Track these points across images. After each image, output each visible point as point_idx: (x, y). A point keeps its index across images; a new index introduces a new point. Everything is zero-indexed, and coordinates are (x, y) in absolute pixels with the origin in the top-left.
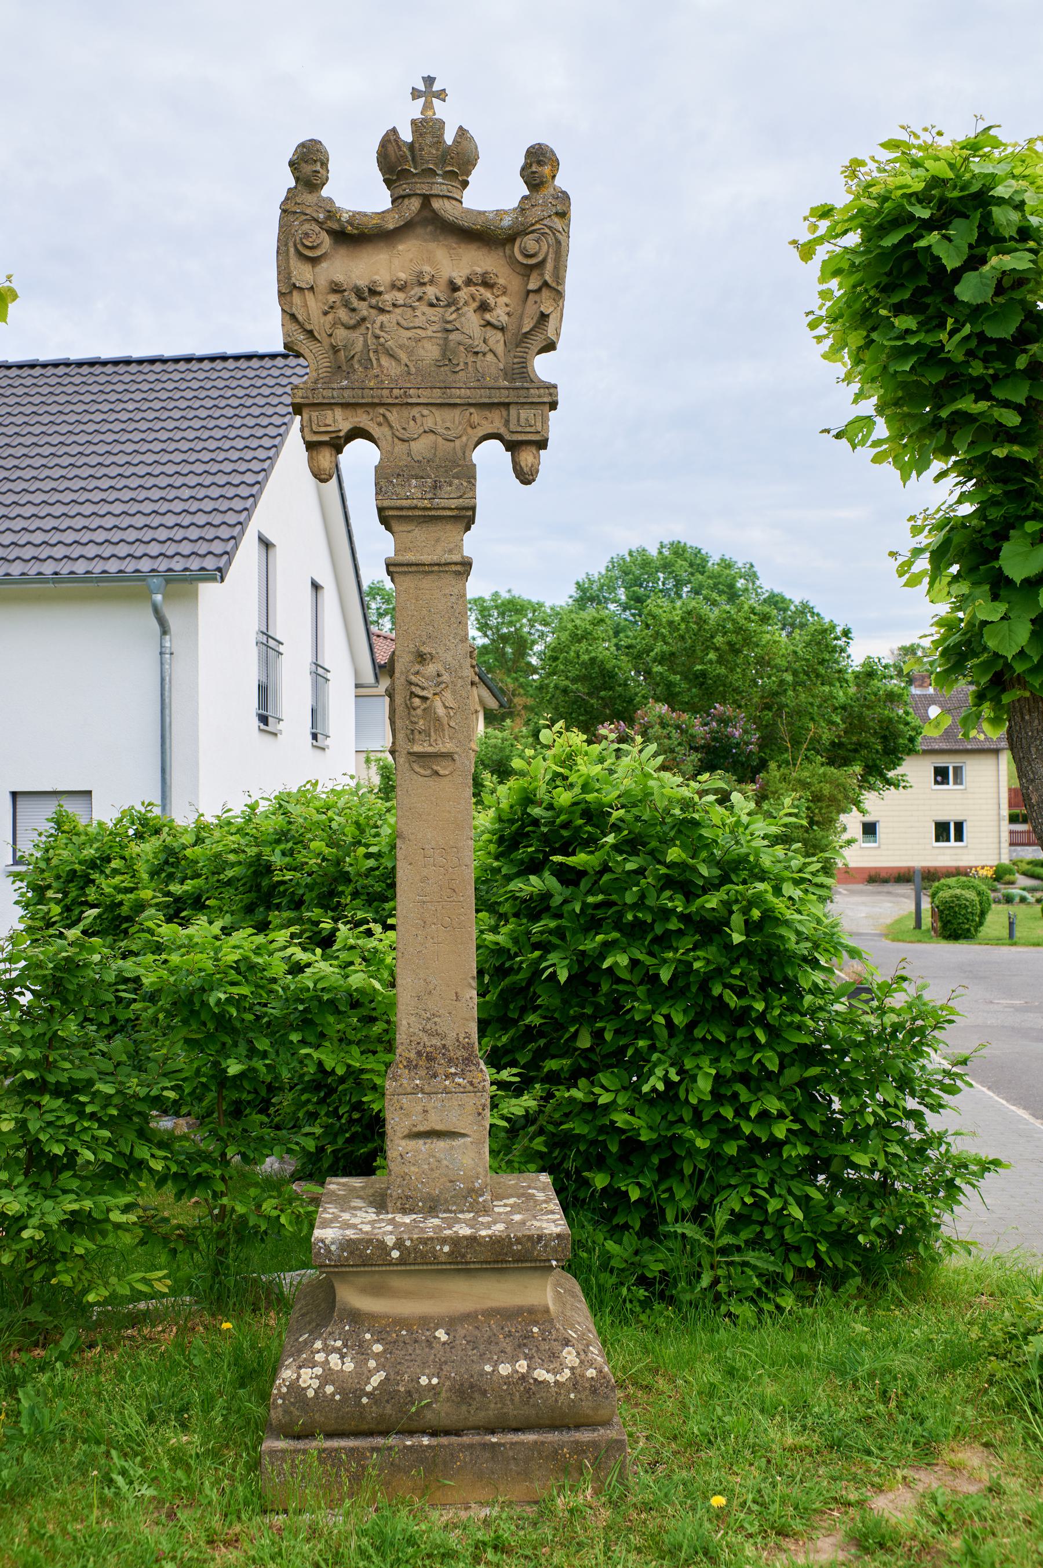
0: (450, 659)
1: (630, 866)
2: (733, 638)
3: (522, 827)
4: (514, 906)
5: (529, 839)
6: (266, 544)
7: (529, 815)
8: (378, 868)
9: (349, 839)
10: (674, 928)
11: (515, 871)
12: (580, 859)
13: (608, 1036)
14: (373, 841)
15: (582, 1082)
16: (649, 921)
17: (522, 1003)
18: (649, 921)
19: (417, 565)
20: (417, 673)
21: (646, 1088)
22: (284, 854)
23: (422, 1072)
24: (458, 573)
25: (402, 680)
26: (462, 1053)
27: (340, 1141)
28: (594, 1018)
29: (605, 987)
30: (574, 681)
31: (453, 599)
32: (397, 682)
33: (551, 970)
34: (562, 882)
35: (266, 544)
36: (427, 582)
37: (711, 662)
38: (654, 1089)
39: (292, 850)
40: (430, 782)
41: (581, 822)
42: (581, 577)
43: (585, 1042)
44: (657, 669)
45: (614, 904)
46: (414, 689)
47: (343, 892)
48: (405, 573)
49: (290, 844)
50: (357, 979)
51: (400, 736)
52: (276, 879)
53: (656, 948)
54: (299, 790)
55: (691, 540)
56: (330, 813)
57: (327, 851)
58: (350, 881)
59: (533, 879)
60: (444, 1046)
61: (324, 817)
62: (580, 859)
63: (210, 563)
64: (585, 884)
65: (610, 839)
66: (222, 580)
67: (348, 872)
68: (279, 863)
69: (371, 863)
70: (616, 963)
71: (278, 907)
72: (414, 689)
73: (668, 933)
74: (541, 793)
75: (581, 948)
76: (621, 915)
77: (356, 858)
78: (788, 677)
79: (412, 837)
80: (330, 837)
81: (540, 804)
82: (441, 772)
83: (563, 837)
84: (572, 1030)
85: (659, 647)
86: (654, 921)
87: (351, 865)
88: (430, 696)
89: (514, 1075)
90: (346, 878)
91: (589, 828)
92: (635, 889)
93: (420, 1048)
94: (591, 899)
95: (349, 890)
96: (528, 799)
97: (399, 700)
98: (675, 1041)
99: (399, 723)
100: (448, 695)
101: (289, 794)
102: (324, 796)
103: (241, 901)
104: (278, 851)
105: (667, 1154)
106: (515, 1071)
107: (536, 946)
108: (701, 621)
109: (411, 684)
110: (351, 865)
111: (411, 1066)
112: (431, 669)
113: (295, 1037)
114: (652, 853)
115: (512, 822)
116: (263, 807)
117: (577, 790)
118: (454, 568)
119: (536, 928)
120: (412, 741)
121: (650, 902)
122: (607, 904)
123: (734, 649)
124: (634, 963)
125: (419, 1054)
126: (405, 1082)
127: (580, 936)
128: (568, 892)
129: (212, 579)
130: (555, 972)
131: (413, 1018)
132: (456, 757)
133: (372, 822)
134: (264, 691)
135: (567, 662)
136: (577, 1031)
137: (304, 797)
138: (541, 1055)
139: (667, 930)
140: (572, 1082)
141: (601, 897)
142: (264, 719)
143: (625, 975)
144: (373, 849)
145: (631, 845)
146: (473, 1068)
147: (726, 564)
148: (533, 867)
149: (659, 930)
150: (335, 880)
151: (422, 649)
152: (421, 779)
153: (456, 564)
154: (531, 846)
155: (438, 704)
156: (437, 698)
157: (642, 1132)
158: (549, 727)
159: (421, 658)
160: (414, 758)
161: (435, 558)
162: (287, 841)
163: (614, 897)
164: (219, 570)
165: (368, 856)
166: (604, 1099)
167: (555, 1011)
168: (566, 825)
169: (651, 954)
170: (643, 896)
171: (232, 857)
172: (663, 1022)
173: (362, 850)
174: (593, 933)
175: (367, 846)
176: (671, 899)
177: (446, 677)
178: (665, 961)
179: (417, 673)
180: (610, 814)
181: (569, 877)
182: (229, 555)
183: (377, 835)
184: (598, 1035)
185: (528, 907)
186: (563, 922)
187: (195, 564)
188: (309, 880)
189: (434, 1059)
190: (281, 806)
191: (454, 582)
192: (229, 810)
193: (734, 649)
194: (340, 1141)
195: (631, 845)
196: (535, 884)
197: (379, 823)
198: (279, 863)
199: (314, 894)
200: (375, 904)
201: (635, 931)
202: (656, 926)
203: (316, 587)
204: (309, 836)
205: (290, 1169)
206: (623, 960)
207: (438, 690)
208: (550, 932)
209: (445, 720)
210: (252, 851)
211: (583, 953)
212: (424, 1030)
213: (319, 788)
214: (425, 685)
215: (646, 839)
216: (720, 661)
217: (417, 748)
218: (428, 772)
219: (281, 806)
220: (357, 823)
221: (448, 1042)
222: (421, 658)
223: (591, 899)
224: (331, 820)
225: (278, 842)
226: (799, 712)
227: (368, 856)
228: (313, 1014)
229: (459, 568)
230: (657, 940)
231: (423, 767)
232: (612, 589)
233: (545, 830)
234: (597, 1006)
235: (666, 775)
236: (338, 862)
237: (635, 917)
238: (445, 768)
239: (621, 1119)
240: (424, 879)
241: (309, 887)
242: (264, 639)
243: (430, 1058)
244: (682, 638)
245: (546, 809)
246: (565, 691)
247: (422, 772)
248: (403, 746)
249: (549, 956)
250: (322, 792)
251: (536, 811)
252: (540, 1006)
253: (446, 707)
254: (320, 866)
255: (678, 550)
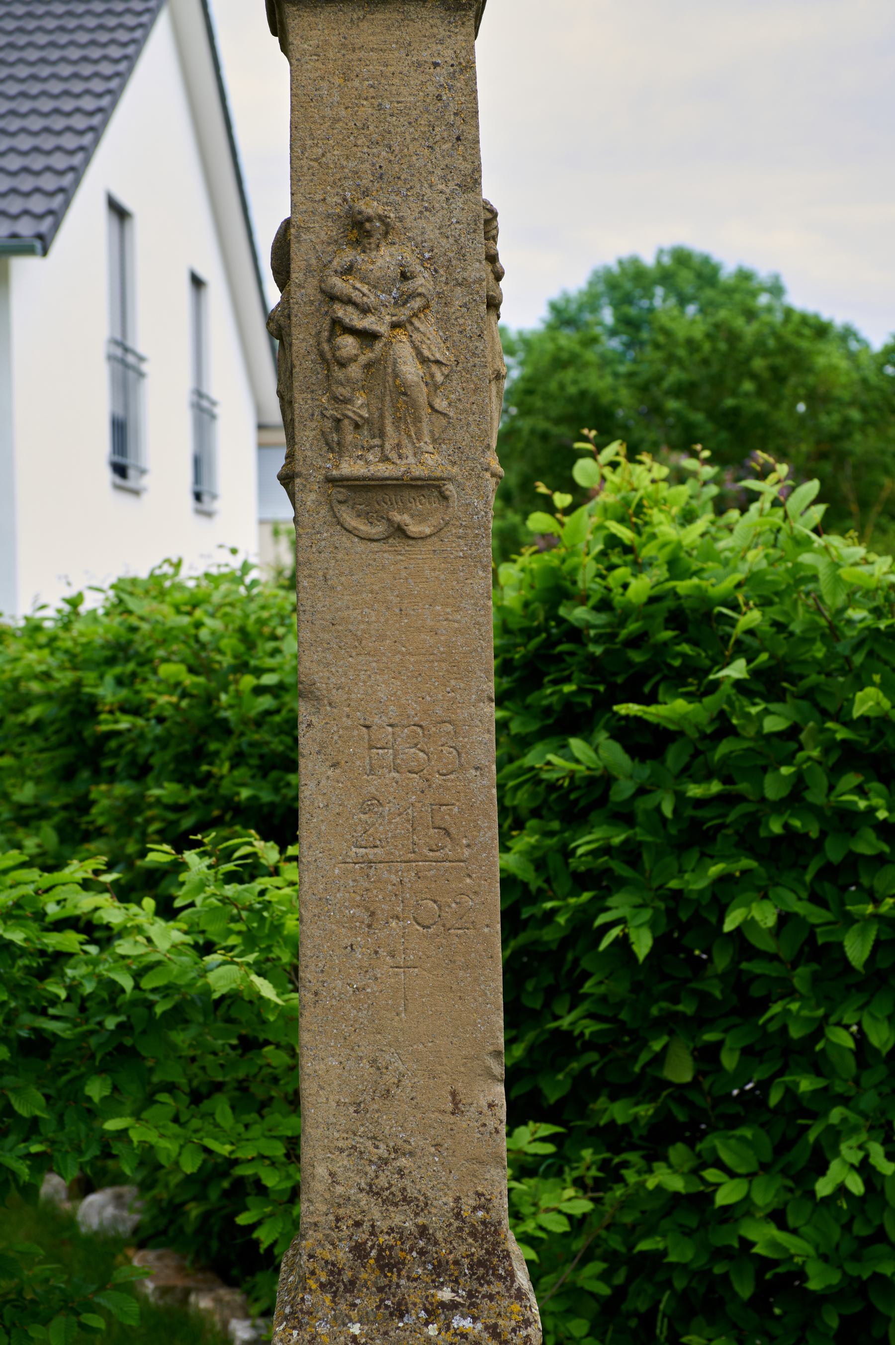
0: (432, 234)
1: (773, 724)
2: (779, 361)
3: (550, 643)
4: (533, 795)
5: (563, 667)
6: (119, 212)
7: (561, 621)
8: (278, 711)
9: (227, 661)
10: (868, 851)
11: (534, 727)
12: (672, 709)
13: (729, 1061)
14: (270, 662)
15: (678, 1152)
16: (814, 834)
17: (549, 980)
18: (814, 834)
20: (348, 270)
21: (824, 1187)
22: (120, 682)
23: (368, 1302)
26: (468, 1248)
27: (214, 1194)
28: (701, 1022)
29: (721, 962)
30: (558, 421)
31: (441, 75)
32: (297, 294)
33: (615, 932)
34: (632, 750)
35: (119, 212)
37: (747, 395)
38: (842, 1190)
39: (134, 675)
41: (668, 634)
42: (554, 294)
43: (681, 1070)
44: (672, 404)
45: (740, 798)
47: (217, 753)
49: (131, 666)
50: (223, 976)
51: (307, 435)
52: (104, 728)
53: (828, 890)
54: (152, 575)
55: (699, 243)
56: (198, 613)
57: (189, 680)
58: (229, 732)
59: (576, 744)
60: (423, 1230)
61: (186, 620)
62: (672, 709)
63: (26, 228)
64: (674, 757)
65: (737, 670)
66: (45, 252)
67: (225, 720)
68: (109, 699)
69: (266, 702)
70: (750, 923)
71: (112, 776)
73: (853, 861)
75: (673, 884)
76: (754, 822)
77: (238, 694)
78: (855, 414)
79: (338, 696)
80: (196, 655)
81: (584, 600)
82: (414, 529)
83: (630, 664)
84: (657, 1046)
85: (675, 375)
86: (823, 834)
87: (231, 706)
88: (383, 329)
89: (543, 1140)
90: (224, 729)
91: (686, 648)
92: (785, 770)
93: (361, 1236)
94: (695, 791)
95: (227, 749)
96: (557, 590)
97: (301, 341)
98: (870, 1079)
99: (302, 402)
100: (427, 327)
101: (134, 581)
102: (191, 584)
103: (52, 759)
104: (109, 678)
105: (857, 1307)
106: (546, 1129)
107: (581, 881)
108: (733, 337)
109: (332, 297)
110: (231, 706)
111: (339, 1285)
112: (385, 259)
113: (96, 1090)
114: (809, 695)
115: (528, 633)
116: (93, 602)
117: (660, 572)
119: (584, 844)
120: (337, 448)
121: (816, 796)
122: (726, 800)
123: (778, 376)
124: (784, 919)
125: (359, 1251)
126: (323, 1329)
127: (670, 861)
128: (645, 771)
129: (29, 251)
130: (626, 937)
131: (344, 1161)
133: (267, 630)
135: (548, 397)
136: (665, 1048)
137: (156, 587)
138: (585, 1088)
139: (851, 854)
140: (654, 1144)
141: (715, 787)
142: (120, 470)
143: (767, 945)
144: (268, 679)
145: (768, 683)
146: (497, 1287)
147: (745, 276)
148: (568, 722)
149: (834, 853)
150: (204, 730)
151: (361, 205)
154: (568, 680)
155: (404, 351)
157: (812, 1269)
158: (593, 455)
159: (359, 230)
160: (341, 493)
162: (127, 660)
163: (743, 787)
164: (40, 237)
165: (259, 691)
166: (728, 1194)
167: (620, 1005)
168: (637, 641)
169: (816, 899)
170: (799, 784)
171: (36, 687)
172: (851, 1044)
173: (248, 681)
174: (695, 854)
175: (259, 672)
176: (860, 790)
177: (423, 282)
178: (849, 920)
180: (733, 623)
181: (645, 741)
182: (57, 216)
183: (276, 652)
184: (707, 1056)
185: (564, 797)
186: (641, 835)
188: (159, 730)
189: (397, 1265)
190: (121, 601)
191: (442, 32)
192: (43, 607)
193: (778, 376)
194: (214, 1194)
195: (768, 683)
196: (584, 755)
197: (280, 631)
198: (109, 699)
199: (168, 755)
200: (274, 774)
201: (785, 854)
202: (828, 844)
203: (197, 282)
204: (160, 653)
205: (132, 1219)
206: (765, 915)
207: (403, 314)
208: (606, 850)
209: (421, 394)
210: (65, 679)
211: (677, 894)
212: (372, 1191)
213: (184, 572)
215: (796, 669)
216: (761, 392)
217: (349, 468)
218: (378, 529)
219: (121, 601)
220: (243, 633)
221: (434, 1220)
222: (359, 230)
223: (695, 791)
224: (198, 625)
225: (111, 661)
226: (866, 465)
227: (259, 691)
228: (135, 1038)
230: (828, 872)
232: (594, 308)
233: (597, 650)
234: (704, 998)
235: (834, 540)
236: (210, 699)
237: (786, 826)
238: (421, 518)
239: (763, 1236)
240: (371, 804)
241: (162, 742)
242: (119, 352)
243: (388, 1263)
244: (705, 362)
245: (597, 609)
246: (545, 437)
247: (364, 528)
248: (315, 462)
249: (611, 902)
250: (189, 576)
251: (579, 614)
252: (586, 996)
253: (424, 361)
254: (176, 707)
255: (682, 257)
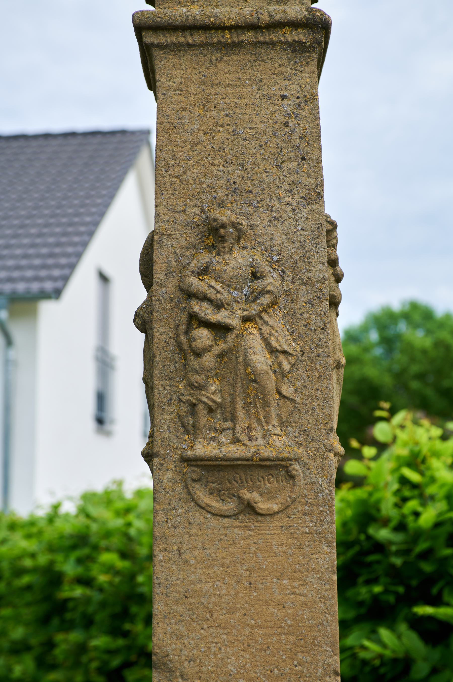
6: (104, 278)
7: (369, 538)
19: (205, 28)
20: (205, 271)
24: (299, 48)
25: (171, 288)
35: (104, 278)
36: (228, 71)
40: (236, 530)
46: (196, 307)
48: (177, 48)
59: (385, 633)
72: (196, 307)
74: (388, 507)
81: (385, 523)
83: (420, 572)
88: (235, 322)
96: (367, 515)
100: (275, 321)
112: (237, 260)
118: (291, 36)
120: (192, 431)
128: (436, 654)
132: (297, 468)
134: (101, 400)
142: (100, 421)
152: (213, 522)
153: (294, 24)
155: (254, 341)
156: (251, 328)
161: (247, 12)
168: (426, 555)
177: (271, 281)
179: (205, 271)
182: (66, 279)
187: (35, 287)
191: (289, 71)
207: (254, 309)
209: (270, 381)
210: (43, 560)
214: (224, 296)
217: (204, 448)
218: (229, 506)
222: (215, 236)
225: (74, 547)
229: (300, 35)
231: (218, 493)
236: (132, 577)
238: (269, 496)
241: (103, 605)
247: (216, 504)
251: (383, 534)
253: (272, 351)
